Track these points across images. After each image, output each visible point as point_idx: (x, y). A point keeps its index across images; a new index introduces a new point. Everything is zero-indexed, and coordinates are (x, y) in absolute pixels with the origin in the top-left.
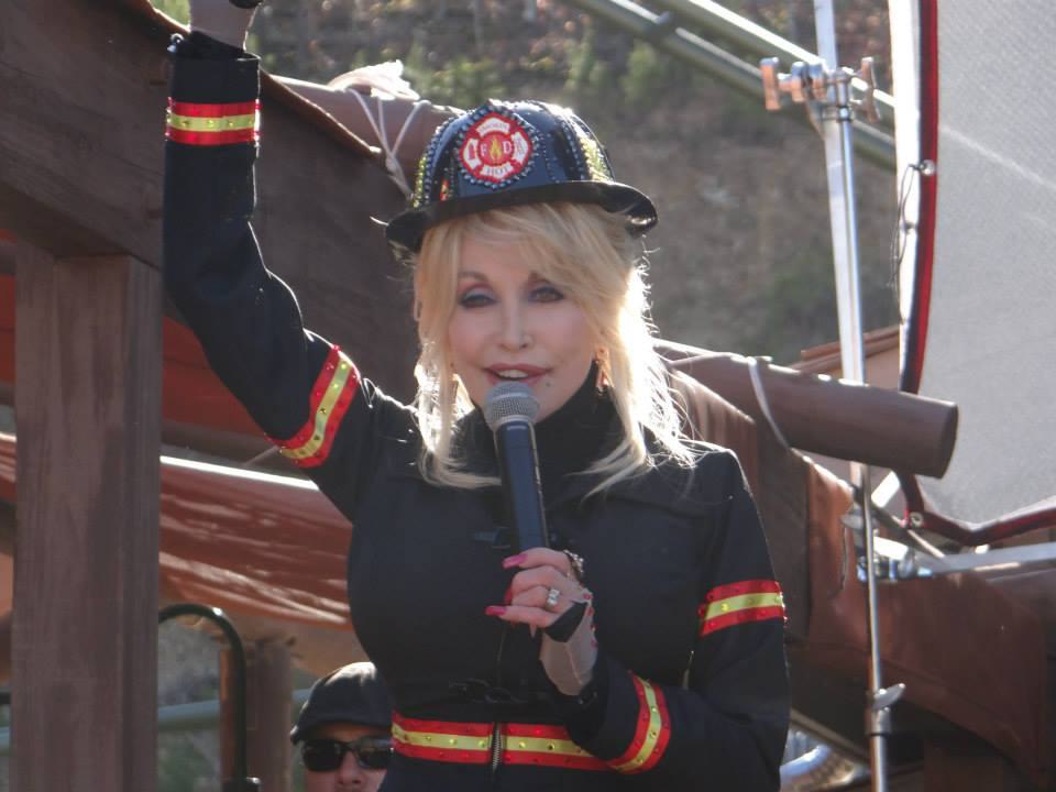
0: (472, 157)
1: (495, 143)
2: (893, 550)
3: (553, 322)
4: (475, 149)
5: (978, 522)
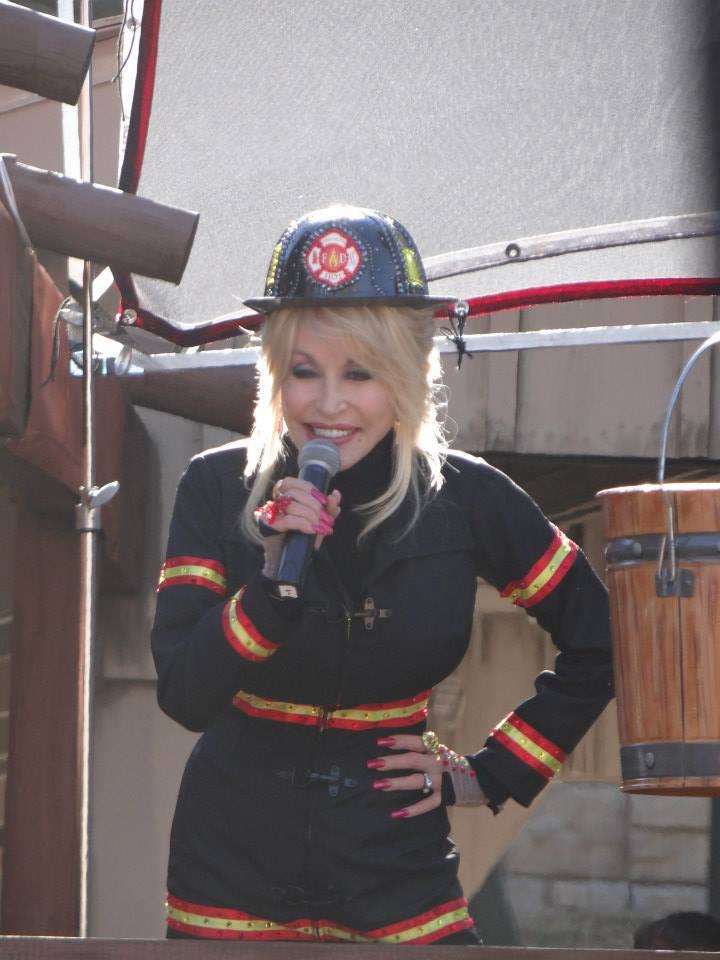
0: (314, 262)
1: (334, 252)
2: (105, 348)
3: (368, 396)
4: (318, 256)
5: (191, 321)
